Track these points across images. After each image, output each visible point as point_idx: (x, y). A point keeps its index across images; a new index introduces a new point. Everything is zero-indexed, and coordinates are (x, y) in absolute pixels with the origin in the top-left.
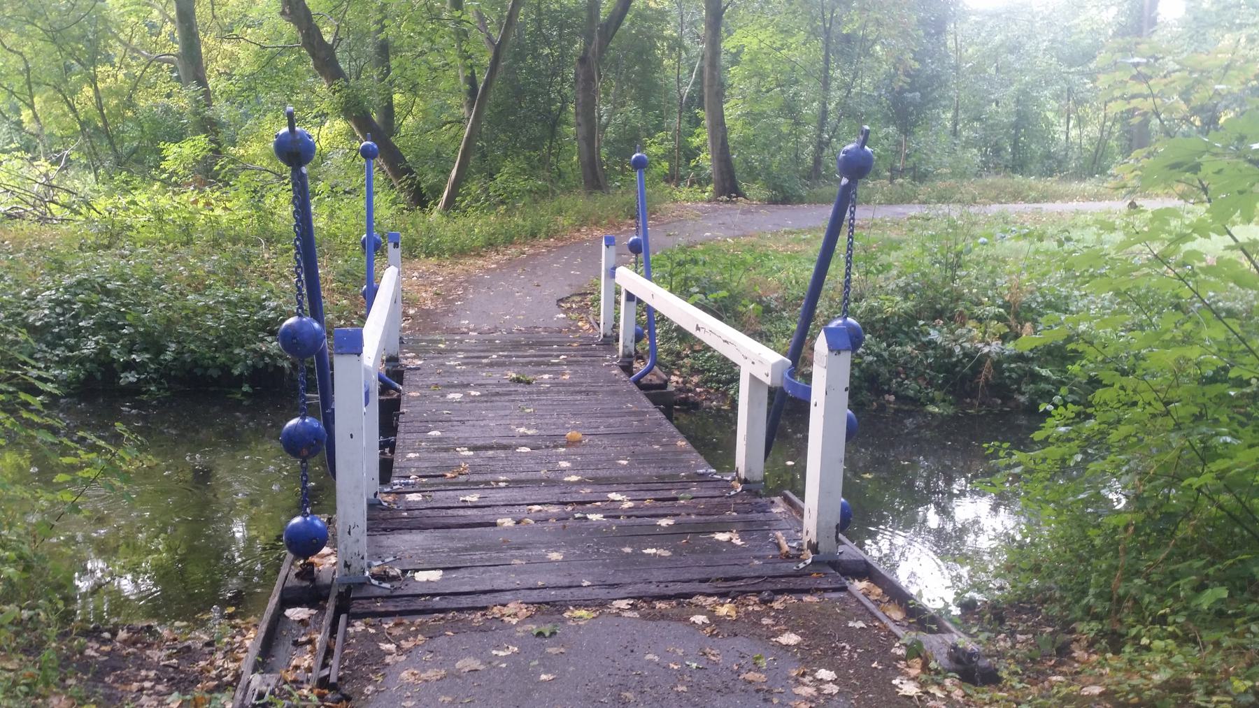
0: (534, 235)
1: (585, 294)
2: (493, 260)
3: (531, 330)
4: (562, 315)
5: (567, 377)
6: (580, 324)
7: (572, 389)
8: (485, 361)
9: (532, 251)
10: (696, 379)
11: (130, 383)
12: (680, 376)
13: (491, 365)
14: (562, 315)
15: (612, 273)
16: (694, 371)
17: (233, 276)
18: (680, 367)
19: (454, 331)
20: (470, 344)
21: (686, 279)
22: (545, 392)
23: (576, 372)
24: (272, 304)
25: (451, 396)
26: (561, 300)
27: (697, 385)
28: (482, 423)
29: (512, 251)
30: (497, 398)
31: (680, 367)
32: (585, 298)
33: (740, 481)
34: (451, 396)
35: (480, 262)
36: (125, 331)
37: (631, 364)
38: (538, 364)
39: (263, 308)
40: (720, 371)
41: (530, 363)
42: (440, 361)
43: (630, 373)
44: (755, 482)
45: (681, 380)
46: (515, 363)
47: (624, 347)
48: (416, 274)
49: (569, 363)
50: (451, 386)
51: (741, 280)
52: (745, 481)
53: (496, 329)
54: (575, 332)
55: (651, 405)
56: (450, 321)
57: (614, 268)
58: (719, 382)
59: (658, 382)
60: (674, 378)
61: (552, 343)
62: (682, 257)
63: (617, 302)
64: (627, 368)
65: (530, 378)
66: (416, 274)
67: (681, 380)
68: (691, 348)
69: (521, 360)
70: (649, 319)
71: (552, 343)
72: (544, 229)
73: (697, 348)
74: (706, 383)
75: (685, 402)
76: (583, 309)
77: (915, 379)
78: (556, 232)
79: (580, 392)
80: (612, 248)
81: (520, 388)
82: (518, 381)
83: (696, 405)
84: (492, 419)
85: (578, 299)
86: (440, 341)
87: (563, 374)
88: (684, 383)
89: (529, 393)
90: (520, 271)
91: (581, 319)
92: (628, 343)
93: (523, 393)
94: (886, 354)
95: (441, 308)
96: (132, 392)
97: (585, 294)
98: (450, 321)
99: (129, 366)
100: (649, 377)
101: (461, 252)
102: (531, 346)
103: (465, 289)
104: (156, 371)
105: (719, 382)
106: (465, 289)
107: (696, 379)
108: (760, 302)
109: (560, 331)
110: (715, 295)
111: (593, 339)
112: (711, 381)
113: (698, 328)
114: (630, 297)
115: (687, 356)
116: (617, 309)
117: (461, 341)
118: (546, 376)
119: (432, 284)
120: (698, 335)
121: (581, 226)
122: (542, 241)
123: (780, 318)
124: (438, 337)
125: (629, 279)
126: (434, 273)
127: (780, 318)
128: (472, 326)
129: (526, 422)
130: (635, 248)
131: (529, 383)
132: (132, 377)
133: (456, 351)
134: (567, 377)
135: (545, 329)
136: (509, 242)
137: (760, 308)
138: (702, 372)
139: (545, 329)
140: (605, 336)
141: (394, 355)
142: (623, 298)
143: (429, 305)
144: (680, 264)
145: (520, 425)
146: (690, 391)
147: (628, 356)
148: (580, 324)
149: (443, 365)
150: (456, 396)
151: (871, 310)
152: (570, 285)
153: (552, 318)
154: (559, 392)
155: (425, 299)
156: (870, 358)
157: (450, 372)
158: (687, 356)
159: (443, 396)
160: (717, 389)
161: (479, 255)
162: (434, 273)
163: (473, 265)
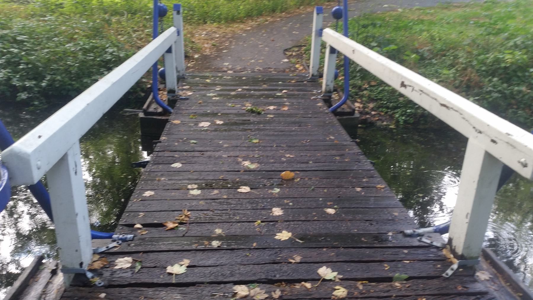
0: (274, 11)
1: (301, 46)
2: (252, 23)
3: (266, 70)
4: (286, 60)
5: (286, 109)
6: (297, 66)
7: (289, 119)
8: (233, 93)
9: (272, 20)
10: (371, 105)
11: (23, 99)
12: (361, 103)
13: (236, 96)
14: (286, 60)
15: (320, 33)
16: (371, 100)
17: (97, 33)
18: (361, 97)
19: (219, 70)
20: (227, 80)
21: (367, 37)
22: (269, 122)
23: (292, 104)
24: (110, 50)
25: (202, 124)
26: (286, 50)
27: (372, 109)
28: (217, 154)
29: (261, 19)
30: (234, 127)
31: (361, 97)
32: (301, 50)
33: (456, 256)
34: (202, 124)
35: (242, 26)
36: (21, 67)
37: (330, 97)
38: (268, 96)
39: (106, 53)
40: (389, 101)
41: (261, 96)
42: (203, 92)
43: (330, 106)
44: (471, 258)
45: (361, 106)
46: (251, 96)
47: (327, 85)
48: (204, 33)
49: (289, 96)
50: (205, 115)
51: (400, 37)
52: (460, 257)
53: (245, 69)
54: (293, 71)
55: (347, 137)
56: (217, 63)
57: (322, 30)
58: (388, 108)
59: (348, 110)
60: (357, 105)
61: (278, 80)
62: (366, 22)
63: (324, 53)
64: (328, 101)
65: (260, 109)
66: (204, 33)
67: (361, 106)
68: (369, 83)
69: (257, 93)
70: (346, 65)
71: (278, 80)
72: (280, 7)
73: (373, 83)
74: (379, 108)
75: (364, 122)
76: (299, 56)
77: (523, 109)
78: (286, 9)
79: (294, 123)
80: (321, 16)
81: (252, 119)
82: (252, 111)
83: (372, 124)
84: (227, 149)
85: (296, 49)
86: (207, 77)
87: (284, 106)
88: (364, 108)
89: (259, 123)
90: (263, 32)
91: (297, 63)
92: (329, 83)
93: (253, 123)
94: (507, 92)
95: (215, 54)
96: (26, 103)
97: (301, 46)
98: (217, 63)
99: (24, 89)
100: (344, 106)
101: (231, 20)
102: (264, 82)
103: (231, 42)
104: (39, 92)
105: (388, 108)
106: (231, 42)
107: (371, 105)
108: (417, 53)
109: (284, 71)
110: (387, 48)
111: (305, 77)
112: (382, 107)
113: (403, 85)
114: (333, 50)
115: (366, 89)
116: (322, 58)
117: (221, 77)
118: (272, 108)
119: (212, 39)
120: (402, 90)
121: (300, 5)
122: (278, 14)
123: (431, 64)
124: (207, 74)
125: (332, 37)
126: (215, 32)
127: (431, 64)
128: (230, 67)
129: (251, 154)
130: (337, 15)
131: (259, 113)
132: (23, 96)
133: (216, 85)
134: (286, 109)
135: (275, 70)
136: (260, 14)
137: (419, 57)
138: (376, 100)
139: (275, 70)
140: (313, 75)
141: (172, 88)
142: (328, 51)
143: (208, 52)
144: (365, 26)
145: (245, 159)
146: (367, 113)
147: (329, 92)
148: (297, 66)
149: (205, 96)
150: (205, 124)
151: (497, 61)
152: (292, 40)
153: (279, 62)
154: (280, 122)
155: (206, 48)
156: (496, 95)
157: (207, 101)
158: (366, 89)
159: (196, 124)
160: (386, 113)
161: (242, 22)
162: (215, 32)
163: (237, 28)
